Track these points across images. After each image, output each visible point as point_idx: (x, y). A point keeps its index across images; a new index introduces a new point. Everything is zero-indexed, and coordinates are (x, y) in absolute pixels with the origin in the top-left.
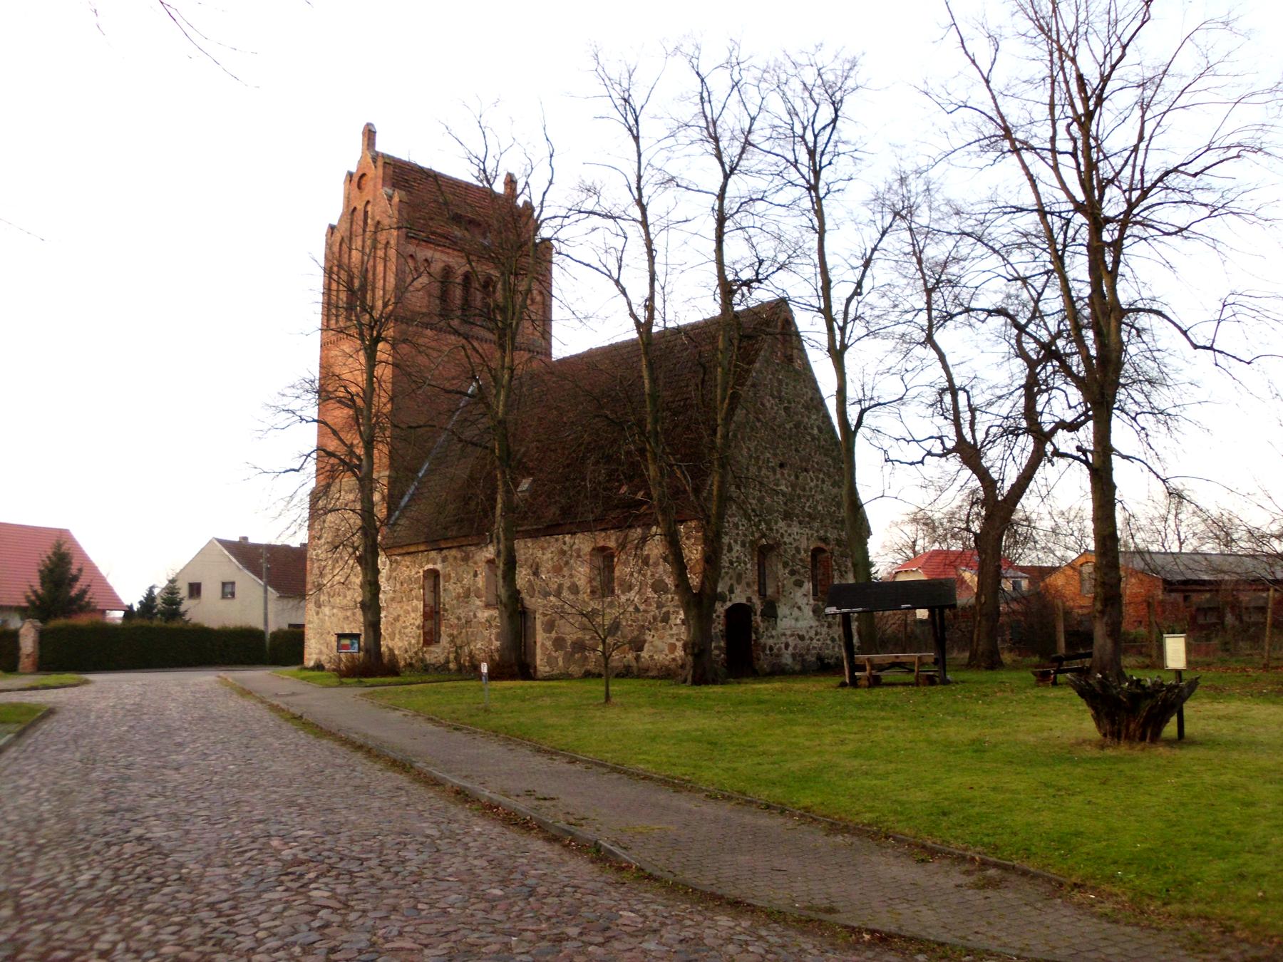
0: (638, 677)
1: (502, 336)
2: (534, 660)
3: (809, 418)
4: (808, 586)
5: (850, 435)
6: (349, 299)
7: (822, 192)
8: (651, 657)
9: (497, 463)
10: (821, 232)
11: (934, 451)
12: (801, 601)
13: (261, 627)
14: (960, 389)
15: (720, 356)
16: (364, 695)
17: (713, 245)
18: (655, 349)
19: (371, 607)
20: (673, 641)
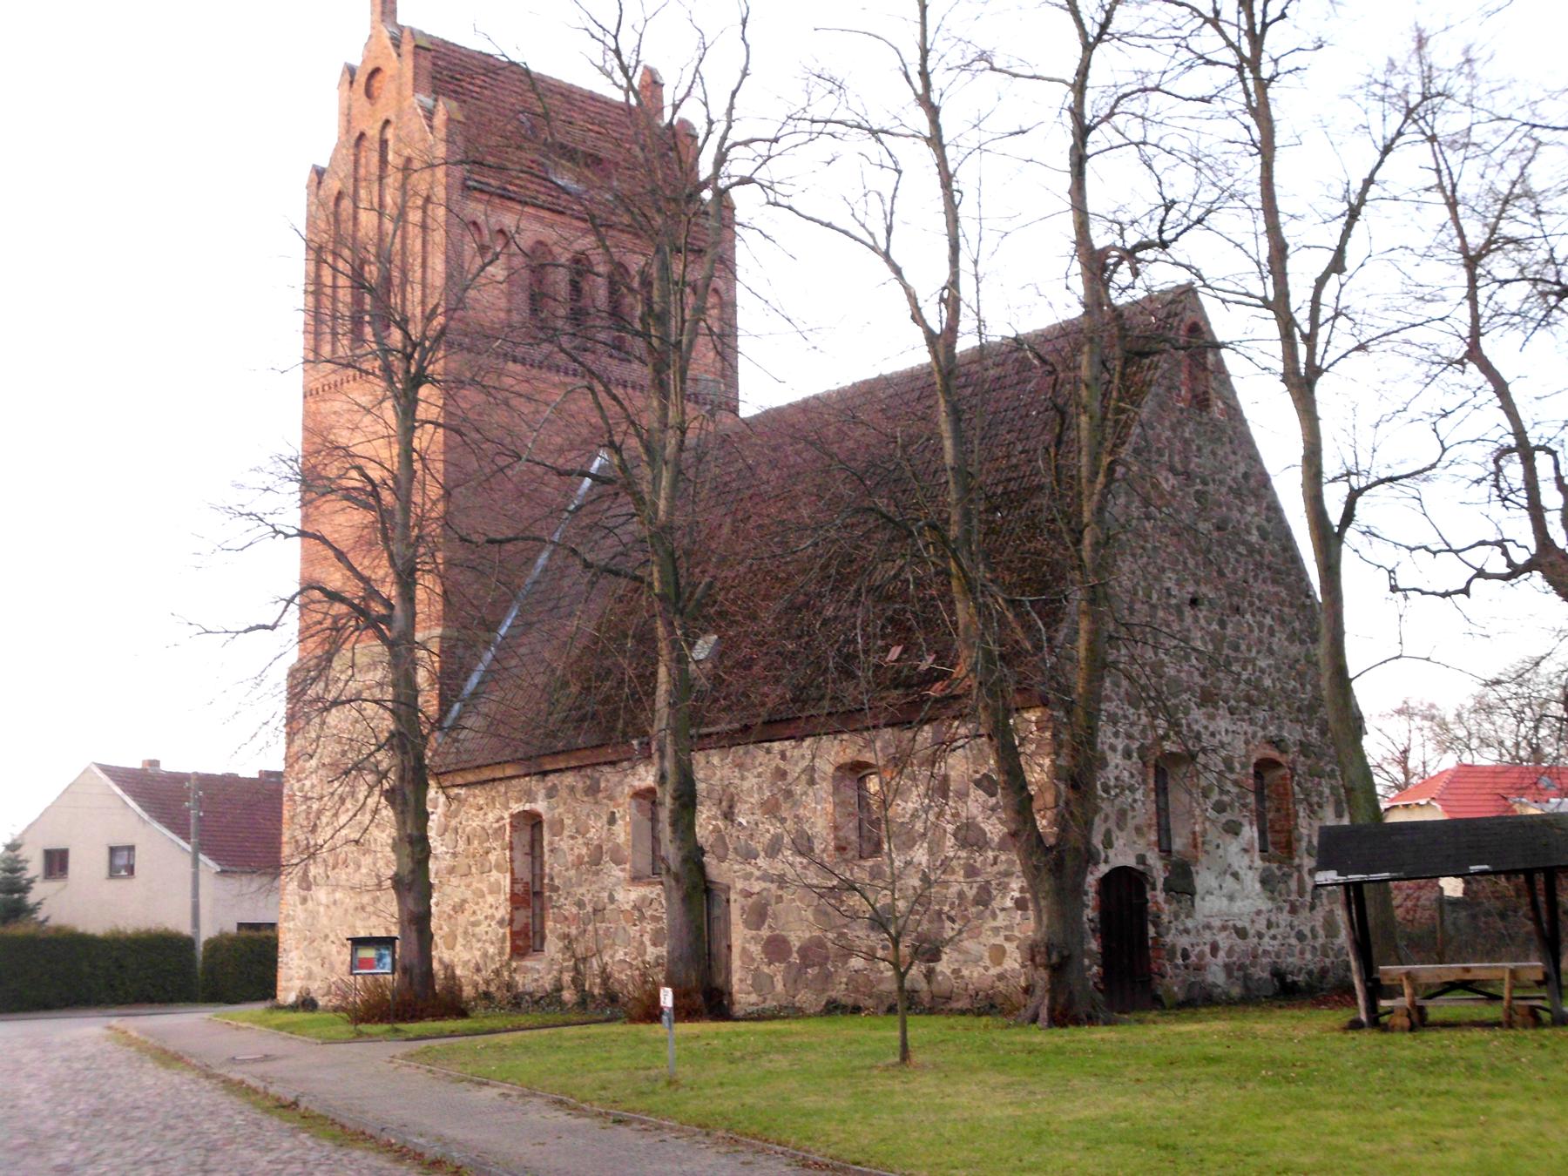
0: (931, 1011)
1: (660, 368)
2: (728, 981)
3: (1242, 511)
4: (1250, 833)
5: (1329, 540)
6: (355, 299)
7: (1266, 73)
8: (956, 972)
9: (658, 607)
10: (1266, 149)
11: (1488, 570)
12: (1240, 863)
13: (186, 930)
14: (1539, 448)
15: (1084, 392)
16: (409, 1056)
17: (1067, 181)
18: (965, 384)
19: (413, 885)
20: (999, 940)
